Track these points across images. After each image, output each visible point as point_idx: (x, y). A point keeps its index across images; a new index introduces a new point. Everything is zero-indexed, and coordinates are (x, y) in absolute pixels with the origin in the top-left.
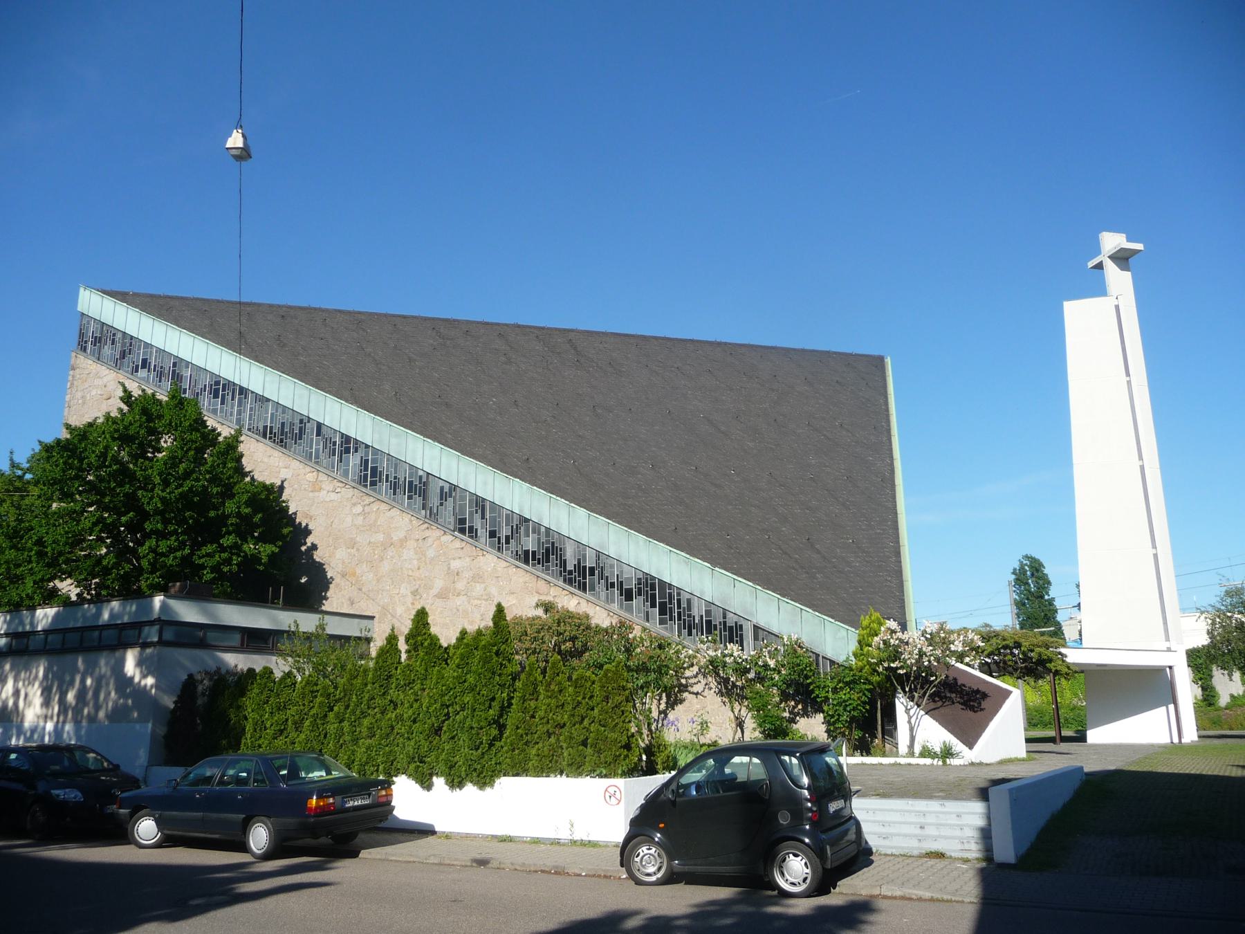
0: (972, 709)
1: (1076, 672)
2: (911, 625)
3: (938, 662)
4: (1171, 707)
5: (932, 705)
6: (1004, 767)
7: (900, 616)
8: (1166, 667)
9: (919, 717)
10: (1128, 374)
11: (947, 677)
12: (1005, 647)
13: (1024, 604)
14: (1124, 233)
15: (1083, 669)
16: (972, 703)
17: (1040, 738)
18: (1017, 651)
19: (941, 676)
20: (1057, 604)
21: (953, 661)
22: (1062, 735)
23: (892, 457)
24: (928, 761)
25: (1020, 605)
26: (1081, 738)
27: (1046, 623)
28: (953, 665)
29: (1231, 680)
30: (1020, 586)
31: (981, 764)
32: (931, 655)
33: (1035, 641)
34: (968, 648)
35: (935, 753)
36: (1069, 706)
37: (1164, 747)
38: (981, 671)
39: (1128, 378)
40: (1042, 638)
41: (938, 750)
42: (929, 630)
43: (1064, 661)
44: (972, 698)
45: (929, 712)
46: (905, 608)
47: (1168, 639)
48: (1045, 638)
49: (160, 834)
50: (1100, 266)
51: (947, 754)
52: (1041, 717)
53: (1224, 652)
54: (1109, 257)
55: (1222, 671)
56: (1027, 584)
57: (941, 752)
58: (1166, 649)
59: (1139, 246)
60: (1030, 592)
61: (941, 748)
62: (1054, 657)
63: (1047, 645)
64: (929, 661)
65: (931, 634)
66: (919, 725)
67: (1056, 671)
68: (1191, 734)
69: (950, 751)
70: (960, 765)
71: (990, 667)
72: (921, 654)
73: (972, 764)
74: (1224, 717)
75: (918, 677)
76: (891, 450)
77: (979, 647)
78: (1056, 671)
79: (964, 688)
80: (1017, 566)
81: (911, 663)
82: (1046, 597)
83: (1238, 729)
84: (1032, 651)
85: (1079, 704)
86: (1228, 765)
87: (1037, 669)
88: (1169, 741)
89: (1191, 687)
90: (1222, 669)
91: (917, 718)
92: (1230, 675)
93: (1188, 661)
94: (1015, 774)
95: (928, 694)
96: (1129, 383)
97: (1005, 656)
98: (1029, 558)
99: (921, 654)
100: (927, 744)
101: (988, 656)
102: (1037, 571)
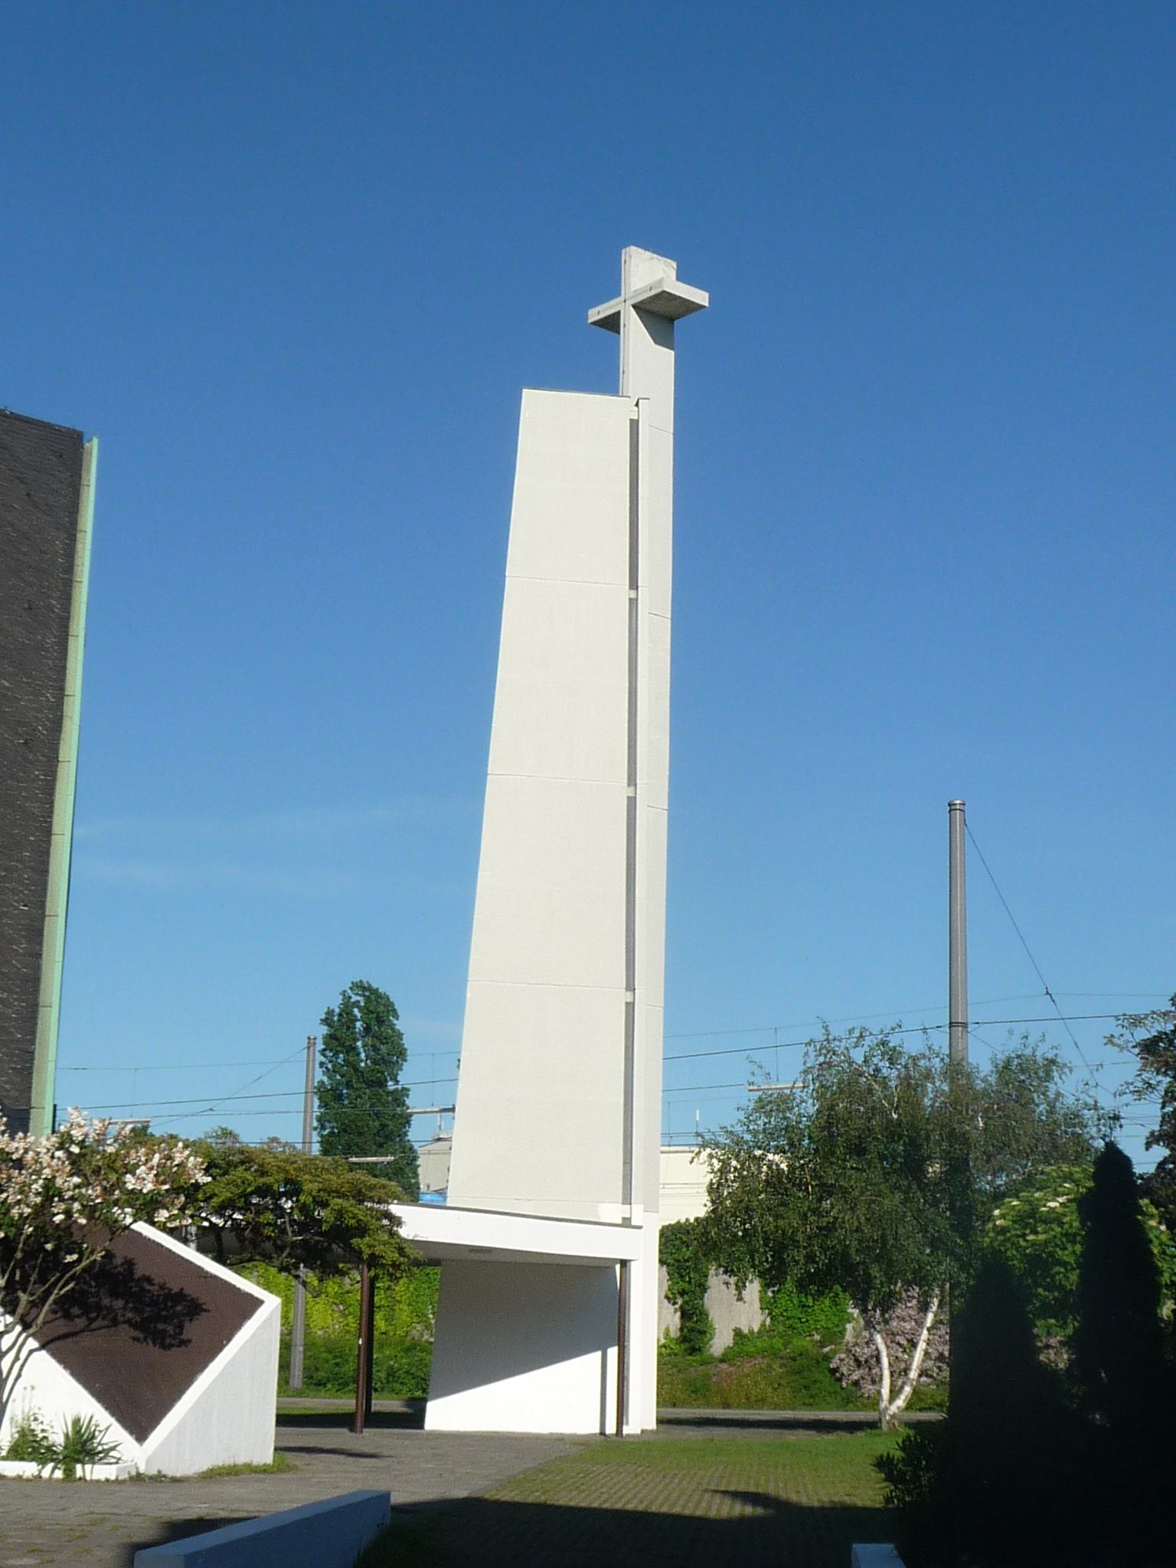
0: (162, 1341)
1: (417, 1263)
2: (42, 1118)
3: (90, 1218)
4: (613, 1352)
5: (62, 1326)
6: (214, 1488)
7: (13, 1093)
8: (615, 1261)
9: (23, 1355)
10: (634, 584)
11: (109, 1256)
12: (263, 1191)
13: (339, 1098)
14: (674, 260)
15: (436, 1256)
16: (160, 1326)
17: (294, 1416)
18: (290, 1204)
19: (92, 1253)
20: (413, 1103)
21: (126, 1216)
22: (373, 1409)
23: (62, 689)
24: (28, 1469)
25: (329, 1096)
26: (414, 1418)
27: (381, 1146)
28: (127, 1227)
29: (740, 1299)
30: (336, 1054)
31: (159, 1479)
32: (73, 1199)
33: (334, 1181)
34: (167, 1187)
35: (49, 1448)
36: (402, 1342)
37: (582, 1443)
38: (201, 1249)
39: (633, 594)
40: (349, 1176)
41: (58, 1439)
42: (77, 1134)
43: (393, 1234)
44: (164, 1313)
45: (52, 1341)
46: (30, 1074)
47: (627, 1199)
48: (360, 1175)
49: (4, 1399)
50: (612, 323)
51: (80, 1453)
52: (337, 1364)
53: (735, 1235)
54: (634, 306)
55: (726, 1277)
56: (353, 1049)
57: (65, 1448)
58: (620, 1221)
59: (700, 297)
60: (356, 1069)
61: (67, 1436)
62: (373, 1224)
63: (360, 1192)
64: (68, 1213)
65: (81, 1144)
66: (19, 1376)
67: (373, 1256)
68: (643, 1416)
69: (89, 1447)
70: (107, 1480)
71: (219, 1239)
72: (50, 1192)
73: (138, 1478)
74: (714, 1379)
75: (34, 1249)
76: (61, 670)
77: (197, 1186)
78: (373, 1256)
79: (147, 1287)
80: (336, 1004)
81: (21, 1215)
82: (391, 1086)
83: (739, 1406)
84: (324, 1205)
85: (426, 1337)
86: (706, 1491)
87: (329, 1250)
88: (597, 1431)
89: (660, 1308)
90: (725, 1272)
91: (17, 1358)
92: (740, 1287)
93: (660, 1251)
94: (233, 1507)
95: (52, 1298)
96: (633, 603)
97: (258, 1213)
98: (364, 989)
99: (50, 1192)
100: (34, 1425)
101: (219, 1211)
102: (380, 1021)
